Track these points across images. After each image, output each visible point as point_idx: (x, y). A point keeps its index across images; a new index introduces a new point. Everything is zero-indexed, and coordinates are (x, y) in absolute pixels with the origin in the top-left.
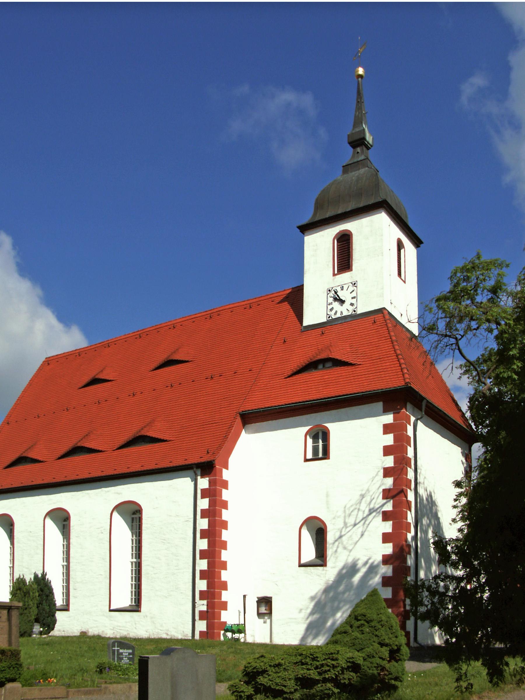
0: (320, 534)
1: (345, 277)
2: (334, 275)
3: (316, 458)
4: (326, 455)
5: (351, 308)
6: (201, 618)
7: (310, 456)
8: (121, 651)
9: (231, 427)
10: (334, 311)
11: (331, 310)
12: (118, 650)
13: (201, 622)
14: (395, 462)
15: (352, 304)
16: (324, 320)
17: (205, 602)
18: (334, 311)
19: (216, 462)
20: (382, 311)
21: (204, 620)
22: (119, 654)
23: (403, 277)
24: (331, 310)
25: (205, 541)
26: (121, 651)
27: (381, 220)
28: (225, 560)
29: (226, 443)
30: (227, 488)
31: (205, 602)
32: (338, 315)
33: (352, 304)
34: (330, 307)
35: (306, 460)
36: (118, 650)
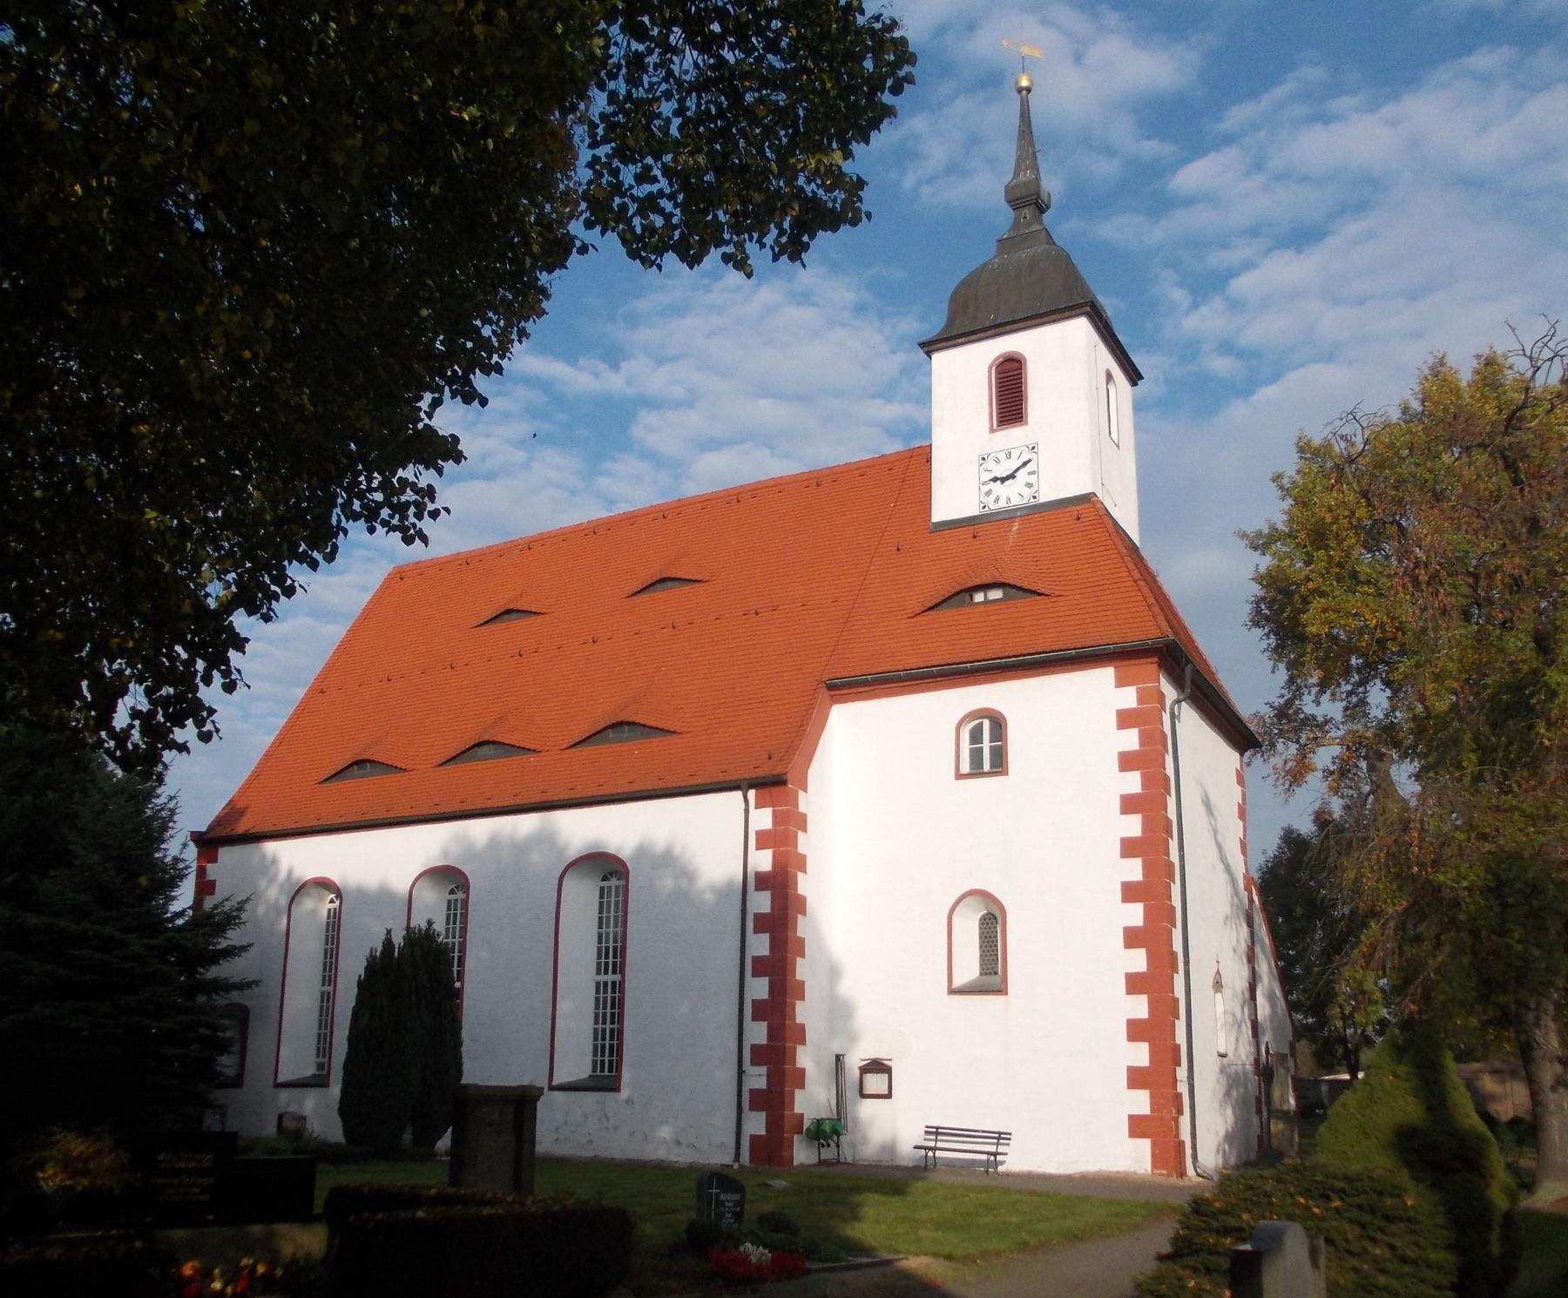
0: (992, 925)
1: (1014, 436)
2: (992, 430)
3: (977, 771)
4: (1000, 764)
5: (1027, 493)
6: (754, 1107)
7: (965, 767)
8: (722, 1197)
9: (811, 707)
10: (992, 497)
11: (988, 493)
12: (717, 1195)
13: (753, 1114)
14: (1144, 785)
15: (1029, 485)
16: (973, 510)
17: (763, 1070)
18: (992, 497)
19: (789, 777)
20: (1088, 499)
21: (761, 1109)
22: (720, 1204)
23: (1114, 435)
24: (988, 493)
25: (765, 938)
26: (722, 1197)
27: (1080, 329)
28: (1133, 951)
29: (800, 735)
30: (805, 830)
31: (763, 1070)
32: (1002, 504)
33: (1029, 485)
34: (985, 489)
35: (959, 776)
36: (717, 1195)
